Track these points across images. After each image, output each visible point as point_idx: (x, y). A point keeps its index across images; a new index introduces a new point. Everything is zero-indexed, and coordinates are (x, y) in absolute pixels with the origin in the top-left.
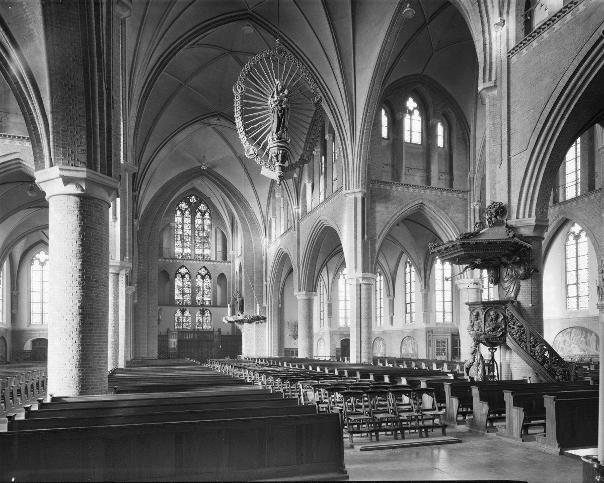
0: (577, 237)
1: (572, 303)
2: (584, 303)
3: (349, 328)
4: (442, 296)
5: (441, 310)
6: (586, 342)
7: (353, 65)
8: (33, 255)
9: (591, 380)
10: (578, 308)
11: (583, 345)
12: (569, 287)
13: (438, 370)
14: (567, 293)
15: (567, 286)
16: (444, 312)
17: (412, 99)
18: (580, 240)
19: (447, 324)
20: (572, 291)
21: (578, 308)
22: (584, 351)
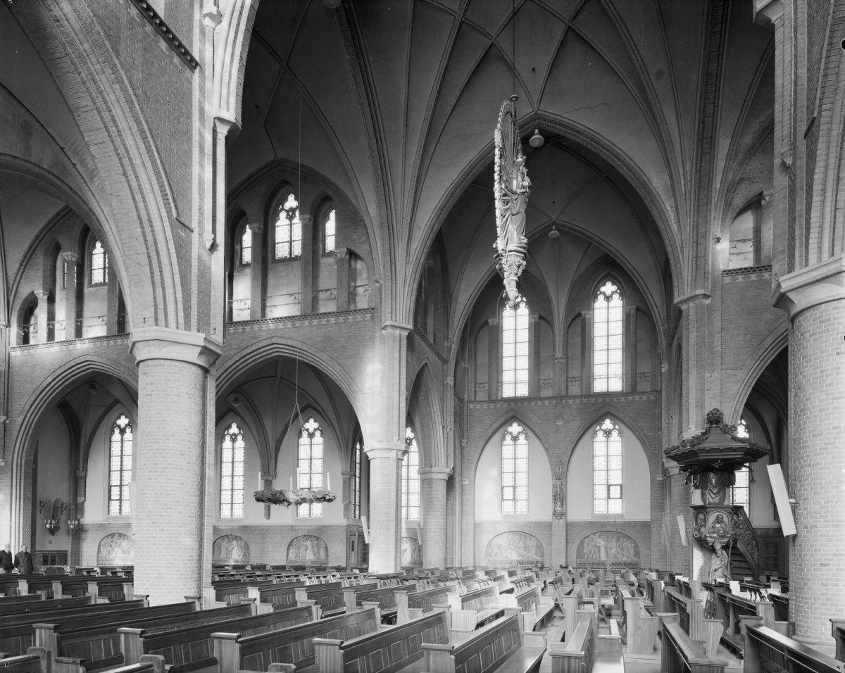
0: (515, 439)
1: (115, 506)
2: (522, 507)
3: (128, 517)
4: (124, 463)
5: (236, 493)
6: (525, 548)
7: (403, 97)
8: (483, 320)
9: (376, 607)
10: (120, 513)
11: (522, 551)
12: (505, 489)
13: (223, 605)
14: (502, 495)
15: (503, 488)
16: (120, 500)
17: (602, 288)
18: (518, 442)
19: (238, 520)
20: (508, 493)
21: (120, 513)
22: (523, 557)
